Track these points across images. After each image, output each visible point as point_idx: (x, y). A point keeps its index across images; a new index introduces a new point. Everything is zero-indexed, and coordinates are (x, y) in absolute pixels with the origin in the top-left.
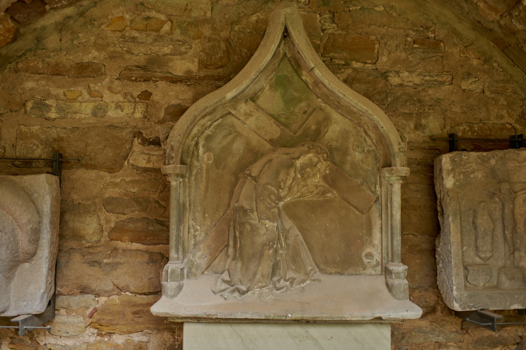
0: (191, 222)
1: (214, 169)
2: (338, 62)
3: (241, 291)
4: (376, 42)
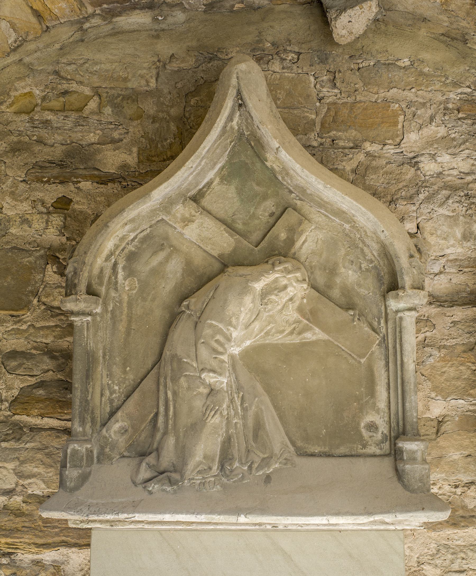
0: (106, 380)
1: (140, 301)
2: (343, 144)
3: (172, 479)
4: (400, 112)
